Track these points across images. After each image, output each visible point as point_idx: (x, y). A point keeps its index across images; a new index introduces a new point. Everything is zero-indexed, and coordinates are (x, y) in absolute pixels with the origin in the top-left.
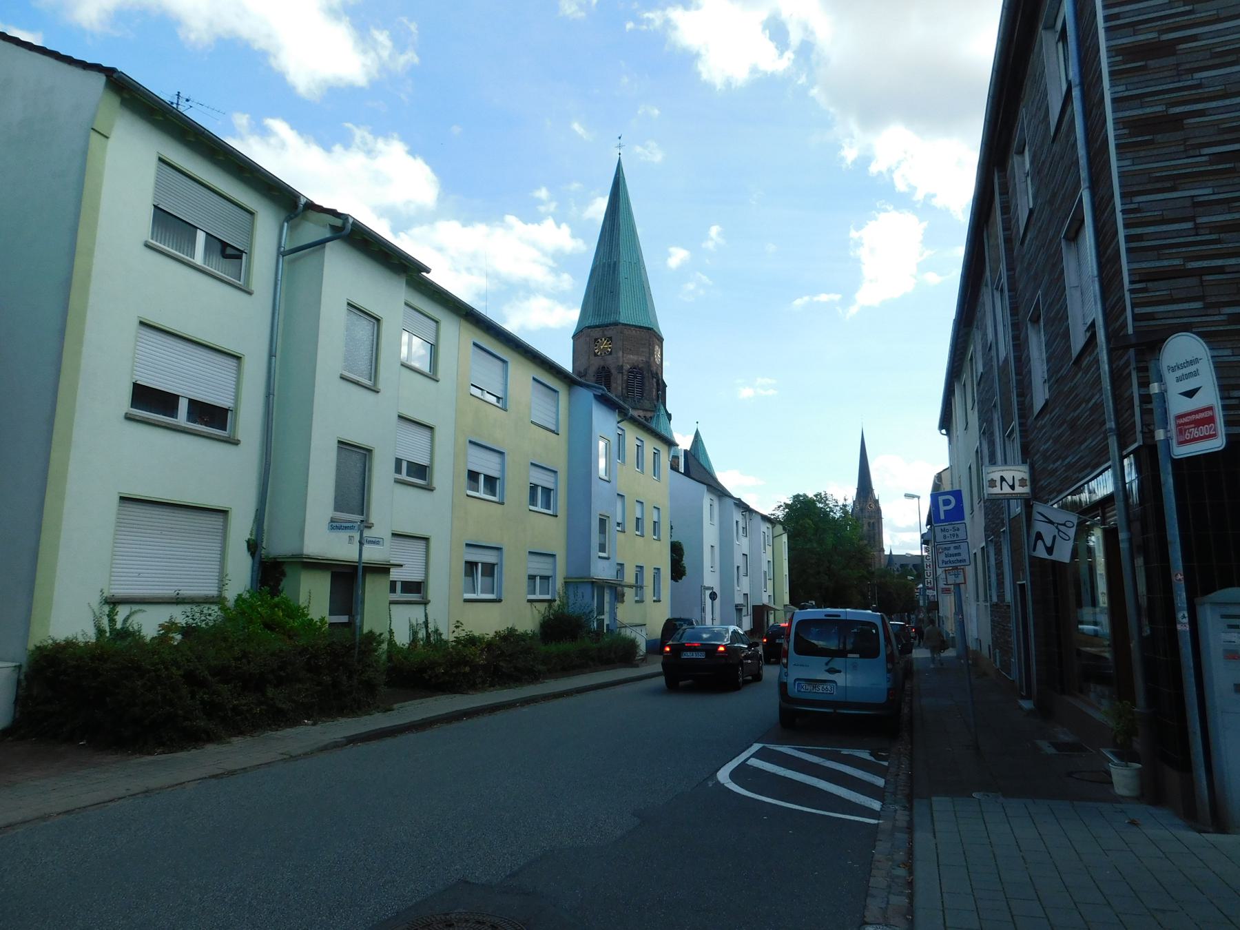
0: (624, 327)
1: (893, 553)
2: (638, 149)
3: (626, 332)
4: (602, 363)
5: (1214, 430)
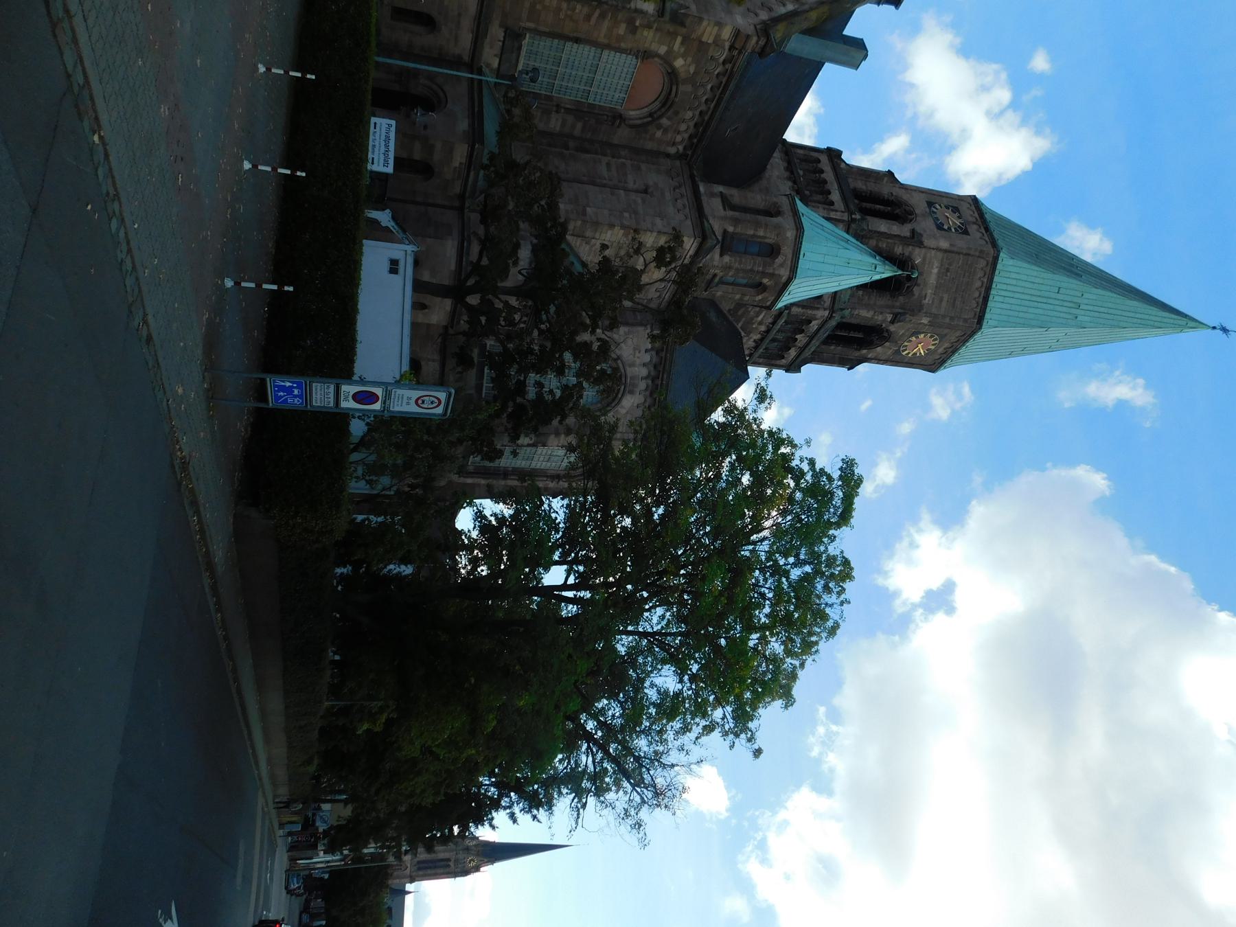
3: (982, 263)
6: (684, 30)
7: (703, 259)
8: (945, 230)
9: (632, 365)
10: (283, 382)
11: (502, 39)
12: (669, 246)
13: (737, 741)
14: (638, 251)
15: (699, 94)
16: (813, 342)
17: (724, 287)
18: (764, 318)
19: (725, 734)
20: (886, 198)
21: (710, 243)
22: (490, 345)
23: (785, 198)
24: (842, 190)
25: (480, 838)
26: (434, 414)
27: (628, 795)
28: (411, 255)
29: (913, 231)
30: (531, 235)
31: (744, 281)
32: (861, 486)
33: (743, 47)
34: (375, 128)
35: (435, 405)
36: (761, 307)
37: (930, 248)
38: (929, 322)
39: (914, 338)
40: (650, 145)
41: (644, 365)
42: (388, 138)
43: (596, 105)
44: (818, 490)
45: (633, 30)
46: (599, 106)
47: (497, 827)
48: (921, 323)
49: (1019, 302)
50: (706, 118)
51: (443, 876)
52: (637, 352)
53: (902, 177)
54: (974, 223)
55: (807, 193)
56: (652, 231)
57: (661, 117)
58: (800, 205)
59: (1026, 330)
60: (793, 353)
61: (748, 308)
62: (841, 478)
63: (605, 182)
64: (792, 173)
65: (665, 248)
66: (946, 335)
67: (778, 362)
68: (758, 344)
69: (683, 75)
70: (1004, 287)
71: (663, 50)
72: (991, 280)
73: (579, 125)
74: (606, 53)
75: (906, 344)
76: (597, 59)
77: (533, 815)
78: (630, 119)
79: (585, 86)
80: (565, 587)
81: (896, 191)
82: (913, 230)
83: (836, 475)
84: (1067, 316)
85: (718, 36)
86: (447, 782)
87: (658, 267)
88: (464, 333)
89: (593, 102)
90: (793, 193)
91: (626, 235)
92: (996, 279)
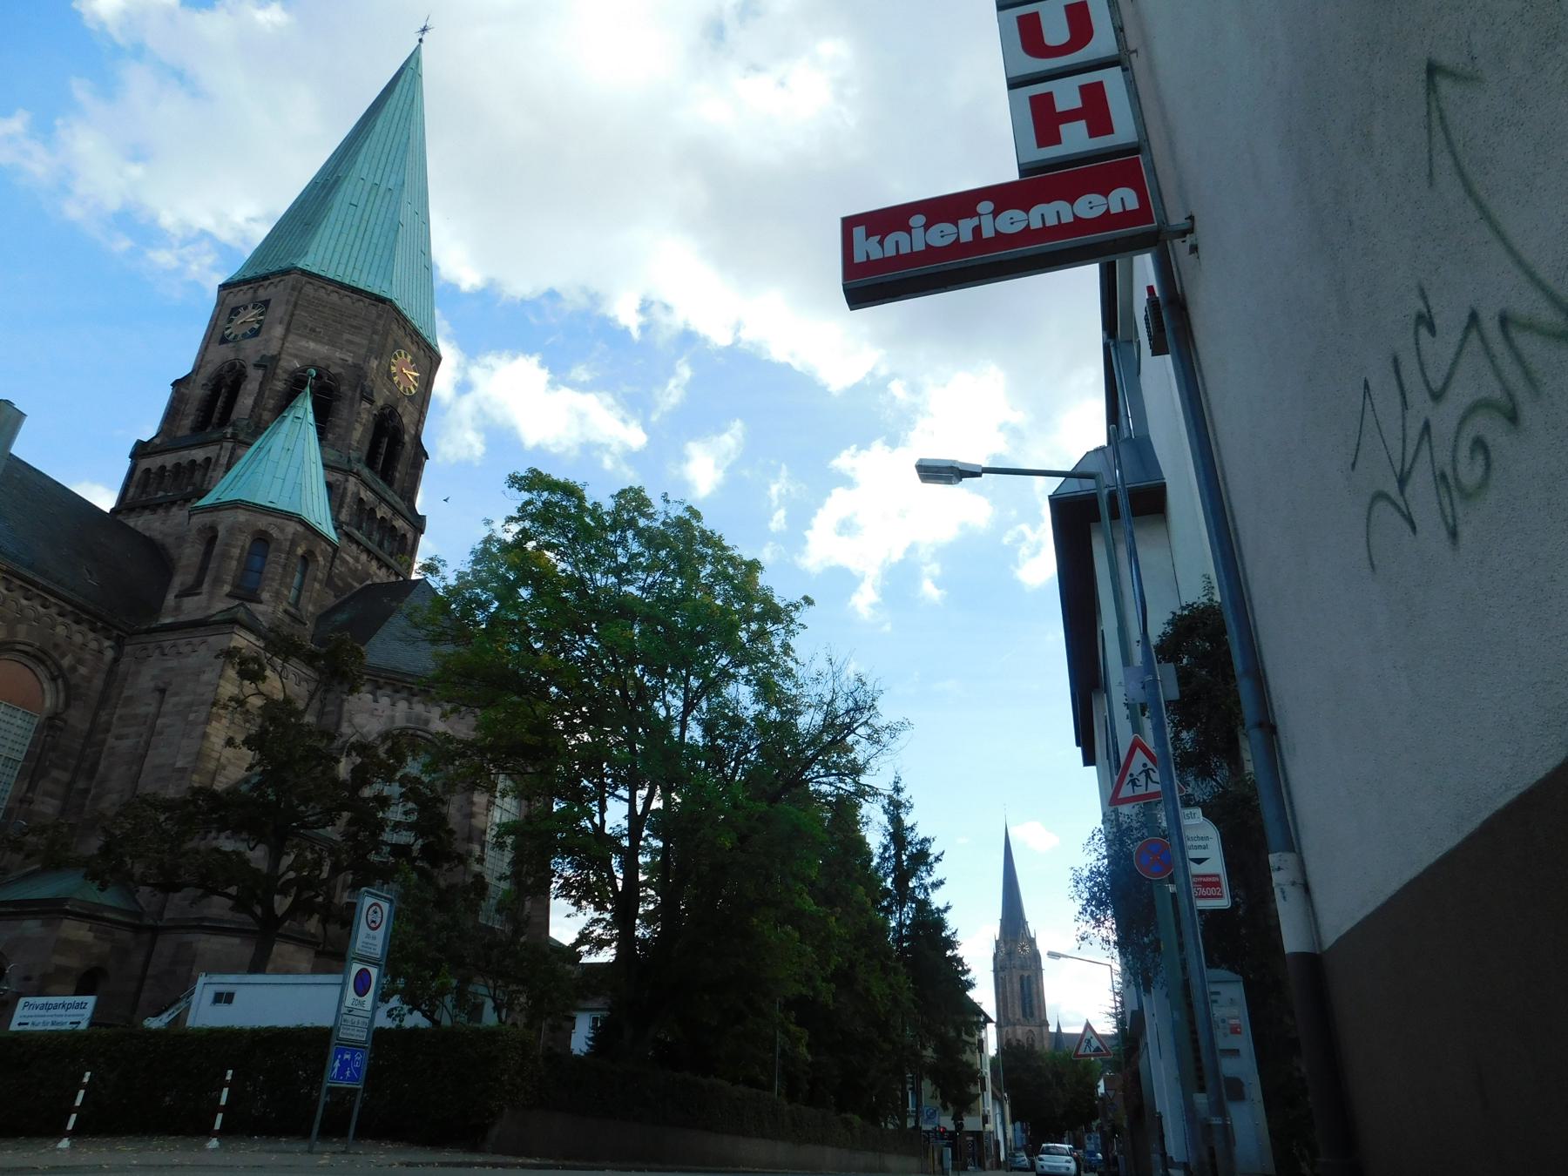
0: (305, 279)
1: (1065, 1030)
2: (598, 374)
4: (232, 356)
5: (1221, 892)
7: (262, 625)
8: (260, 328)
9: (392, 718)
10: (333, 1069)
12: (239, 663)
13: (798, 621)
14: (241, 702)
16: (388, 498)
17: (303, 600)
18: (353, 557)
19: (790, 632)
20: (209, 393)
21: (241, 614)
22: (349, 897)
23: (194, 519)
24: (192, 446)
25: (997, 938)
26: (390, 911)
27: (861, 739)
28: (211, 978)
29: (257, 366)
30: (205, 839)
31: (298, 576)
32: (540, 470)
34: (27, 1024)
35: (378, 909)
36: (334, 557)
37: (282, 348)
38: (376, 359)
39: (395, 379)
40: (98, 683)
41: (393, 705)
42: (46, 1007)
43: (28, 751)
44: (545, 517)
46: (30, 746)
48: (377, 369)
49: (363, 252)
50: (69, 608)
51: (1040, 985)
52: (376, 713)
53: (185, 369)
54: (255, 292)
55: (190, 489)
56: (218, 686)
57: (59, 668)
58: (207, 500)
60: (399, 523)
61: (335, 573)
62: (529, 491)
63: (142, 743)
64: (159, 505)
65: (240, 669)
66: (395, 341)
67: (410, 542)
68: (382, 564)
70: (342, 267)
72: (331, 281)
73: (55, 773)
75: (401, 388)
77: (935, 861)
80: (632, 802)
81: (201, 379)
82: (255, 365)
83: (526, 496)
84: (387, 199)
86: (883, 958)
87: (264, 678)
88: (324, 921)
89: (24, 754)
90: (189, 506)
91: (220, 717)
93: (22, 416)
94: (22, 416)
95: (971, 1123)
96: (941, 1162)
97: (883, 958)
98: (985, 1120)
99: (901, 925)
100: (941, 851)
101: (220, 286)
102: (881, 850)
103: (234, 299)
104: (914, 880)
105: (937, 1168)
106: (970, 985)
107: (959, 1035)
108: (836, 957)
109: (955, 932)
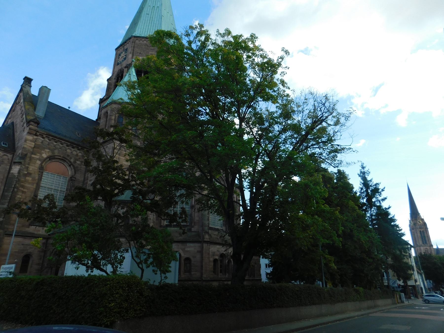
0: (135, 39)
6: (29, 155)
8: (126, 57)
11: (35, 227)
15: (59, 147)
22: (167, 223)
33: (35, 130)
45: (29, 174)
47: (389, 206)
49: (152, 27)
50: (69, 144)
54: (124, 48)
57: (70, 162)
59: (163, 23)
69: (50, 154)
71: (39, 162)
72: (143, 37)
74: (42, 185)
76: (45, 188)
78: (72, 174)
79: (58, 192)
81: (114, 77)
85: (31, 141)
86: (364, 227)
92: (143, 36)
93: (50, 90)
94: (50, 90)
95: (410, 283)
96: (400, 298)
97: (364, 227)
98: (416, 281)
99: (372, 215)
100: (384, 187)
101: (115, 49)
102: (360, 190)
103: (119, 52)
104: (374, 199)
105: (399, 301)
106: (403, 235)
107: (401, 253)
108: (341, 228)
109: (394, 216)
